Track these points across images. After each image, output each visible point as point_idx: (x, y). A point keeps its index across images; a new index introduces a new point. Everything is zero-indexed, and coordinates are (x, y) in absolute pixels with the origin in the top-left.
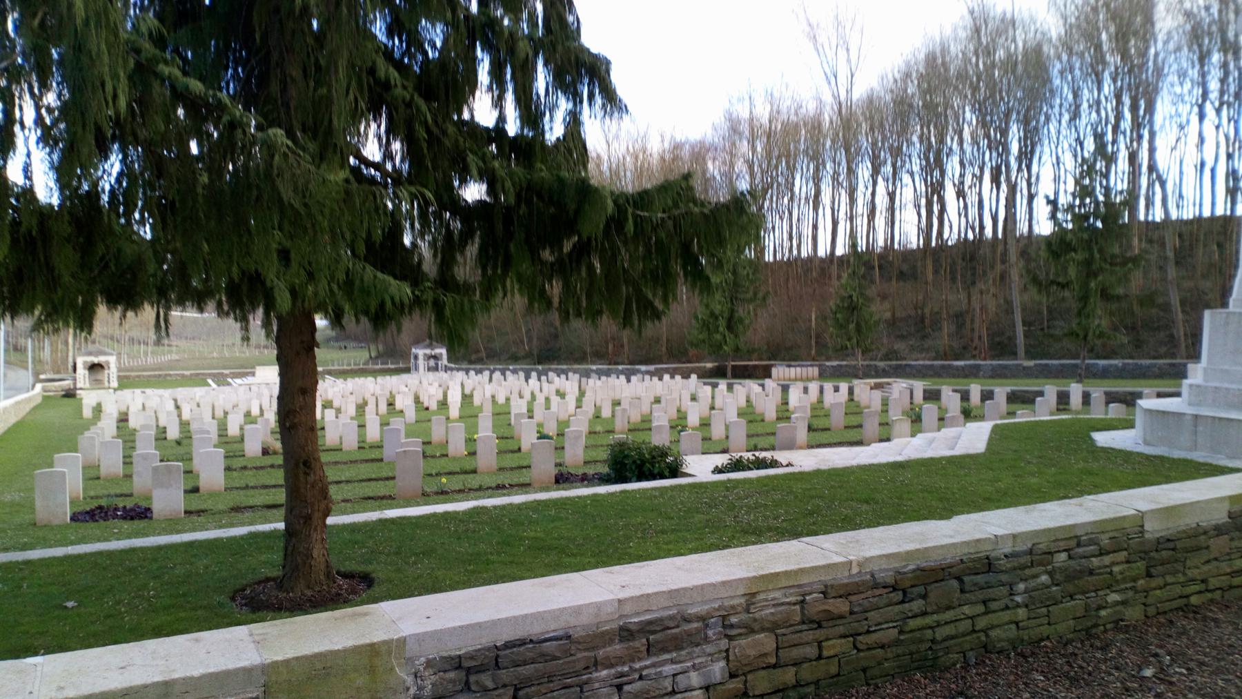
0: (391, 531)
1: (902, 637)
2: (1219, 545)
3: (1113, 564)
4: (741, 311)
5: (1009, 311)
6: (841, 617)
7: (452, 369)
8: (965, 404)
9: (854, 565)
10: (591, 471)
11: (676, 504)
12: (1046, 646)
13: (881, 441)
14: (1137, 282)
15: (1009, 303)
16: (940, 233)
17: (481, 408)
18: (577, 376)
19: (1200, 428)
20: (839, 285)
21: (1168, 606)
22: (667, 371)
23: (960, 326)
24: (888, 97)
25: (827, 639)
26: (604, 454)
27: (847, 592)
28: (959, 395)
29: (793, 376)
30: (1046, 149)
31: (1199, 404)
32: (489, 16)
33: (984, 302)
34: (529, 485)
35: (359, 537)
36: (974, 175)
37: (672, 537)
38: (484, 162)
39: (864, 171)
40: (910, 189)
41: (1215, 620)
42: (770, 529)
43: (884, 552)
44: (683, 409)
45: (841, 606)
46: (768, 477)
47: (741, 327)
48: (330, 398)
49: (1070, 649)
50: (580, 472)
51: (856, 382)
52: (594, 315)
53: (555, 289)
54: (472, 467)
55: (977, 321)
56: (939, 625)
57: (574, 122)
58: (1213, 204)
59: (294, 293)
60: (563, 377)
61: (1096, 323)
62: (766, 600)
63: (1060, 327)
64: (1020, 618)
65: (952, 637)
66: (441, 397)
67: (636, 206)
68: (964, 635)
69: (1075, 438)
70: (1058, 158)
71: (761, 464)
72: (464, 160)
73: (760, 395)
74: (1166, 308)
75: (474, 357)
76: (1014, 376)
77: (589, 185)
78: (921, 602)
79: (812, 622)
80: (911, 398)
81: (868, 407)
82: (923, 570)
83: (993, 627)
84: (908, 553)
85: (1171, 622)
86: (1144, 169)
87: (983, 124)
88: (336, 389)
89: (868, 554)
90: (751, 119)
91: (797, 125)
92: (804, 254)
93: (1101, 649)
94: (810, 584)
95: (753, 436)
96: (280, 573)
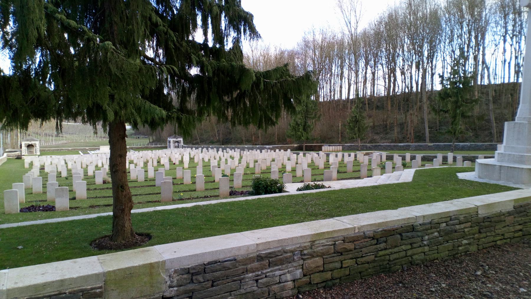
0: (159, 215)
1: (376, 259)
2: (509, 220)
3: (465, 228)
4: (309, 122)
5: (423, 122)
6: (351, 250)
7: (185, 147)
8: (404, 161)
9: (356, 228)
10: (245, 190)
11: (281, 204)
12: (436, 262)
13: (368, 177)
14: (477, 110)
15: (423, 119)
16: (394, 90)
18: (239, 150)
19: (502, 171)
20: (351, 111)
21: (487, 245)
22: (277, 148)
23: (402, 129)
24: (372, 32)
25: (345, 260)
26: (250, 183)
27: (353, 240)
29: (331, 150)
30: (439, 54)
31: (502, 161)
33: (412, 118)
34: (218, 196)
35: (145, 218)
37: (279, 217)
39: (362, 64)
40: (381, 71)
41: (507, 251)
42: (321, 214)
43: (369, 223)
44: (284, 164)
45: (351, 246)
46: (320, 192)
48: (132, 159)
49: (446, 263)
50: (240, 191)
51: (358, 152)
52: (246, 124)
53: (230, 113)
54: (194, 189)
56: (392, 254)
57: (237, 41)
58: (509, 77)
59: (116, 114)
60: (233, 150)
62: (319, 244)
63: (444, 129)
64: (426, 251)
65: (397, 259)
67: (264, 77)
68: (402, 258)
69: (450, 175)
70: (444, 58)
71: (317, 187)
72: (190, 58)
73: (318, 158)
74: (489, 121)
75: (194, 142)
76: (424, 150)
77: (245, 68)
82: (385, 231)
83: (414, 254)
85: (489, 252)
86: (480, 63)
88: (135, 156)
89: (362, 224)
92: (336, 98)
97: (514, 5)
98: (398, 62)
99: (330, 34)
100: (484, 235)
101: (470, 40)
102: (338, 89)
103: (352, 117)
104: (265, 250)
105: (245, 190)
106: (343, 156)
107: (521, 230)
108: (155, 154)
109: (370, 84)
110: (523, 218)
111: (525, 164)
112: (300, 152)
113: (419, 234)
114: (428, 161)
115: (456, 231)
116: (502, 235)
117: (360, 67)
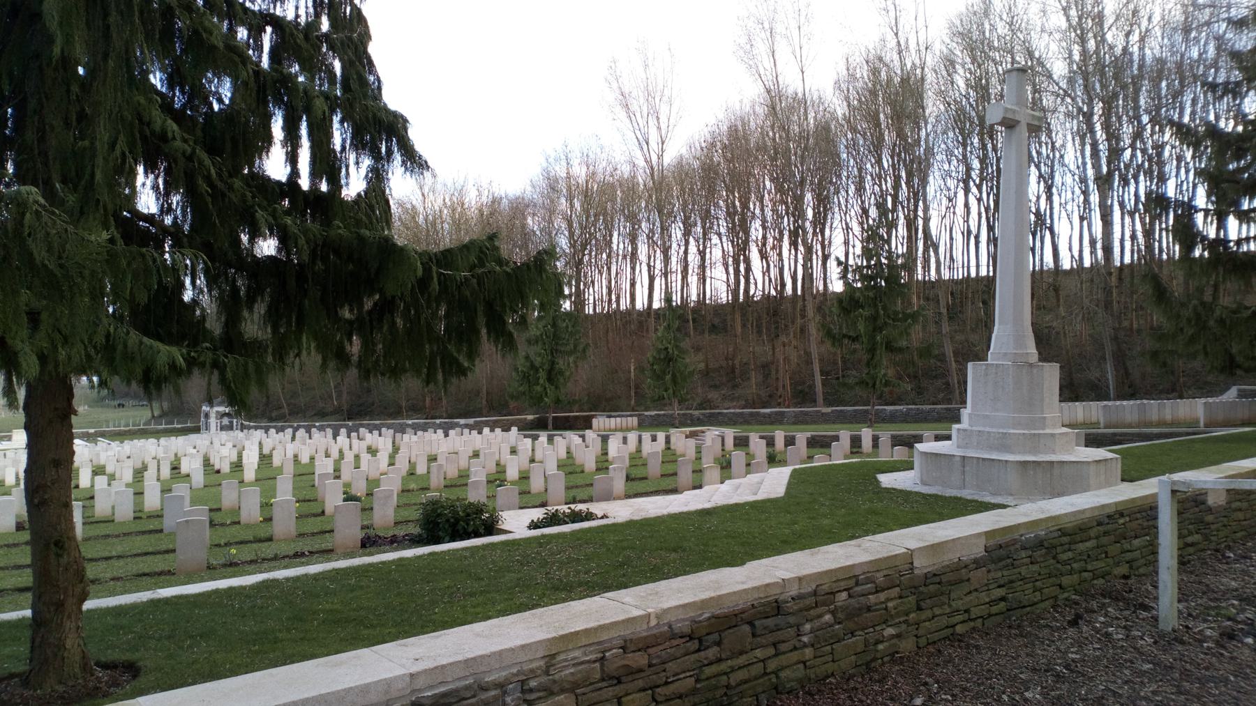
2: (979, 576)
3: (888, 600)
4: (561, 362)
5: (809, 362)
6: (641, 671)
7: (249, 428)
9: (652, 617)
10: (401, 532)
12: (831, 683)
13: (695, 488)
14: (916, 336)
15: (808, 354)
17: (280, 470)
18: (391, 431)
19: (967, 468)
20: (655, 336)
21: (936, 636)
22: (486, 424)
23: (767, 376)
24: (696, 164)
25: (627, 694)
26: (416, 514)
27: (644, 644)
28: (764, 442)
30: (837, 216)
31: (966, 447)
32: (281, 73)
34: (332, 551)
36: (775, 238)
37: (481, 599)
38: (275, 218)
39: (677, 232)
40: (718, 249)
41: (977, 647)
42: (580, 584)
43: (681, 602)
44: (502, 463)
45: (640, 660)
47: (562, 380)
48: (102, 462)
50: (390, 534)
51: (672, 431)
52: (395, 373)
53: (355, 347)
55: (781, 371)
56: (733, 670)
57: (377, 179)
58: (978, 266)
59: (42, 358)
60: (376, 433)
61: (883, 372)
62: (566, 660)
63: (853, 376)
65: (746, 682)
66: (234, 458)
67: (439, 265)
68: (756, 678)
70: (847, 224)
71: (576, 517)
72: (253, 216)
73: (580, 446)
74: (942, 358)
75: (274, 414)
76: (814, 422)
77: (395, 245)
78: (715, 649)
79: (611, 678)
80: (723, 445)
81: (684, 455)
83: (783, 668)
84: (703, 601)
85: (939, 651)
86: (920, 234)
87: (780, 189)
88: (109, 453)
89: (666, 605)
90: (569, 177)
91: (612, 186)
92: (623, 307)
93: (879, 681)
94: (610, 640)
95: (572, 487)
96: (27, 668)
97: (982, 120)
98: (753, 230)
99: (604, 164)
100: (928, 614)
101: (897, 186)
102: (626, 286)
103: (659, 351)
104: (431, 687)
105: (402, 533)
106: (640, 441)
107: (1003, 599)
108: (166, 447)
109: (695, 278)
110: (1005, 573)
111: (1013, 453)
112: (541, 433)
113: (792, 620)
114: (822, 446)
115: (869, 609)
116: (966, 611)
117: (674, 239)
